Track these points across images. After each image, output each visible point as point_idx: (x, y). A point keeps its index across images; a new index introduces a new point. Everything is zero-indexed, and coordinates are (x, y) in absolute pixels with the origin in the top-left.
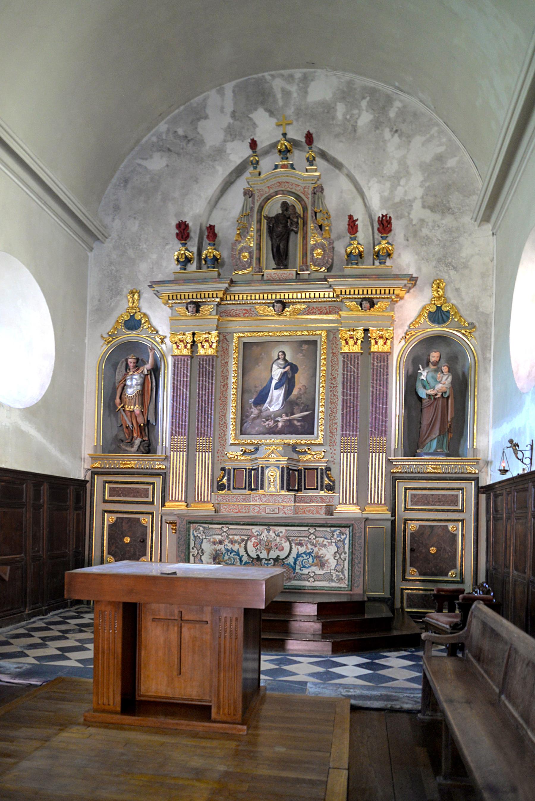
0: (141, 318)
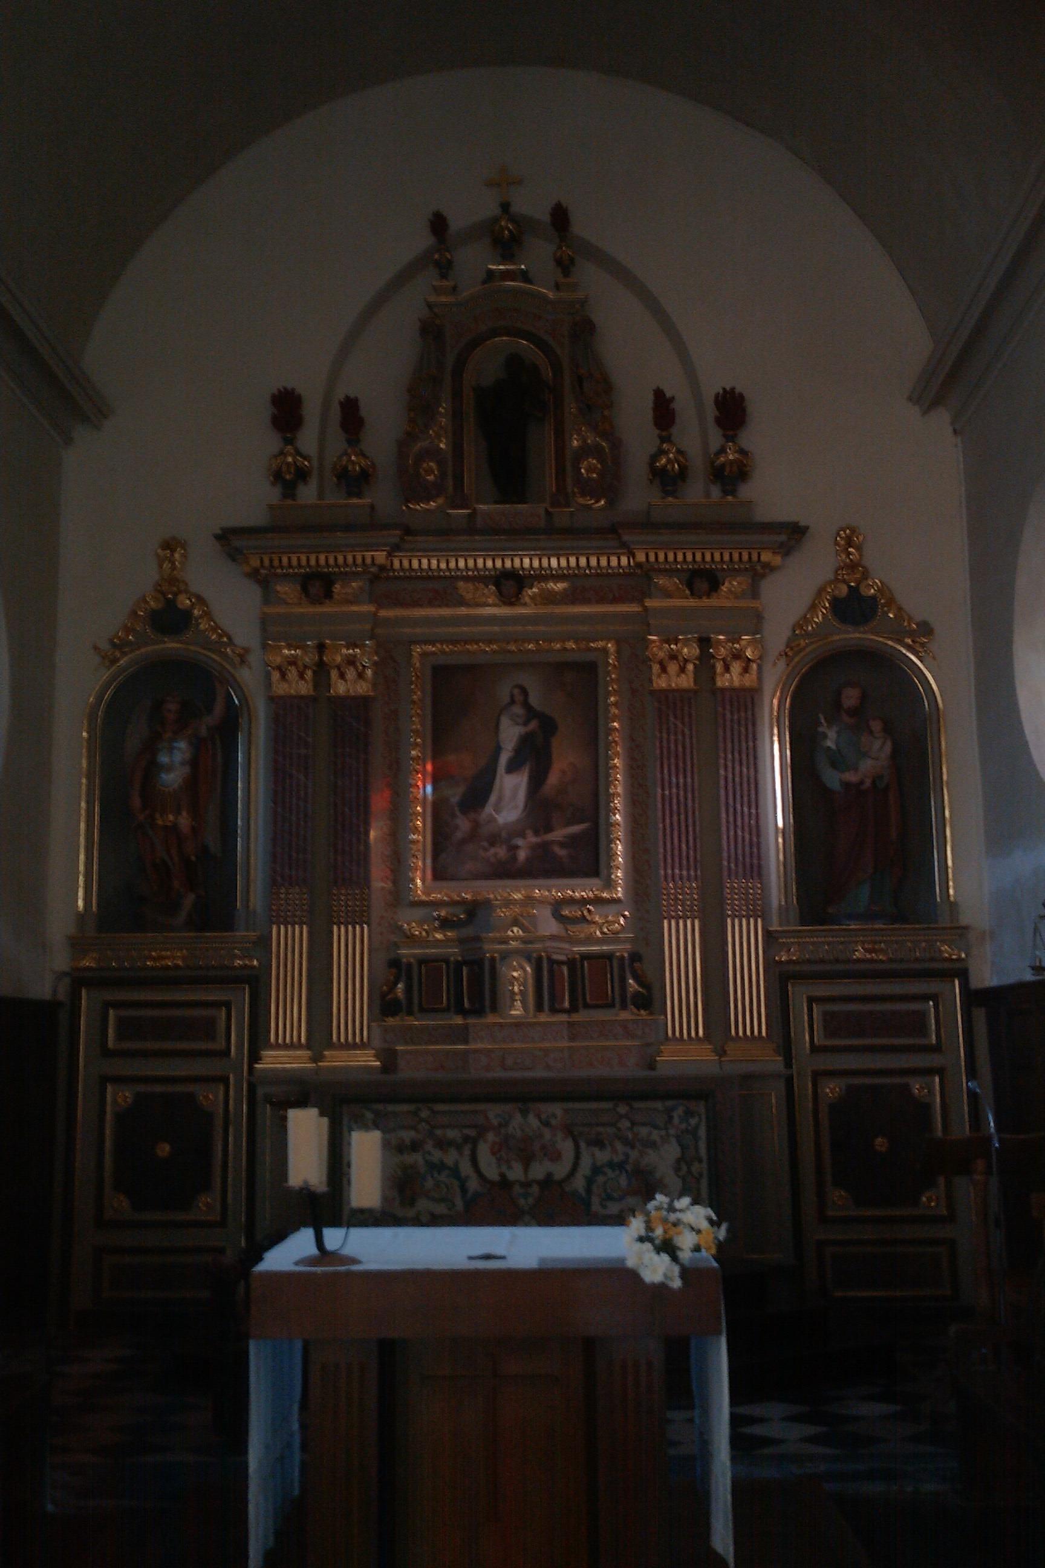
0: (193, 604)
